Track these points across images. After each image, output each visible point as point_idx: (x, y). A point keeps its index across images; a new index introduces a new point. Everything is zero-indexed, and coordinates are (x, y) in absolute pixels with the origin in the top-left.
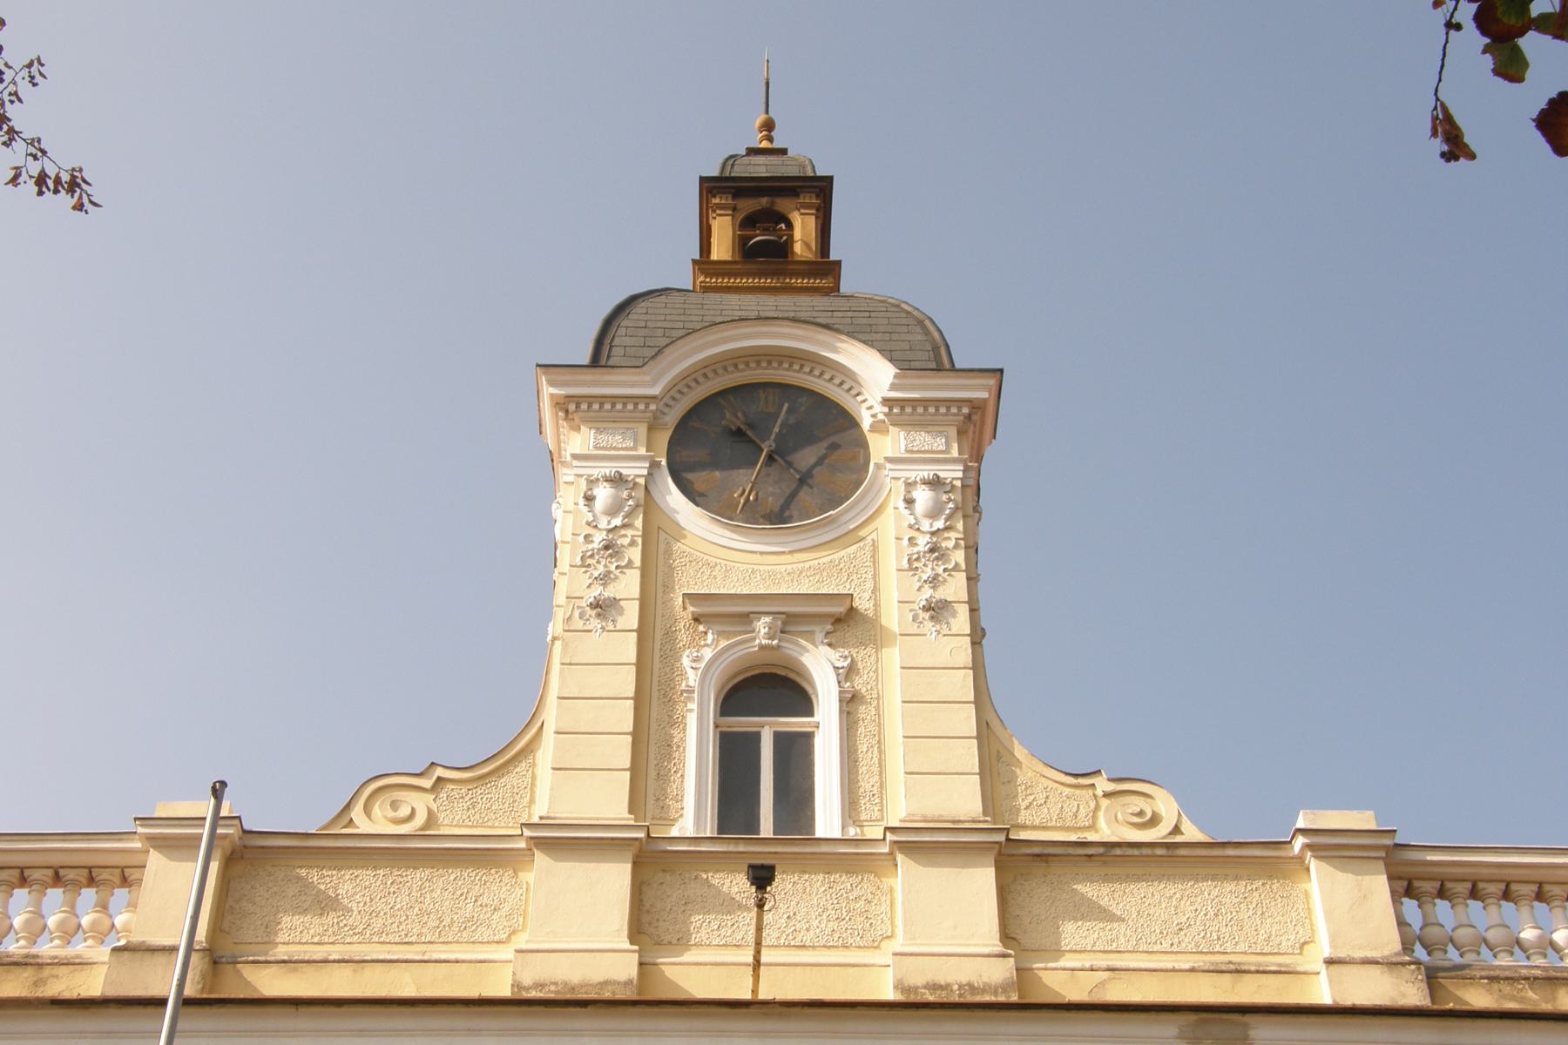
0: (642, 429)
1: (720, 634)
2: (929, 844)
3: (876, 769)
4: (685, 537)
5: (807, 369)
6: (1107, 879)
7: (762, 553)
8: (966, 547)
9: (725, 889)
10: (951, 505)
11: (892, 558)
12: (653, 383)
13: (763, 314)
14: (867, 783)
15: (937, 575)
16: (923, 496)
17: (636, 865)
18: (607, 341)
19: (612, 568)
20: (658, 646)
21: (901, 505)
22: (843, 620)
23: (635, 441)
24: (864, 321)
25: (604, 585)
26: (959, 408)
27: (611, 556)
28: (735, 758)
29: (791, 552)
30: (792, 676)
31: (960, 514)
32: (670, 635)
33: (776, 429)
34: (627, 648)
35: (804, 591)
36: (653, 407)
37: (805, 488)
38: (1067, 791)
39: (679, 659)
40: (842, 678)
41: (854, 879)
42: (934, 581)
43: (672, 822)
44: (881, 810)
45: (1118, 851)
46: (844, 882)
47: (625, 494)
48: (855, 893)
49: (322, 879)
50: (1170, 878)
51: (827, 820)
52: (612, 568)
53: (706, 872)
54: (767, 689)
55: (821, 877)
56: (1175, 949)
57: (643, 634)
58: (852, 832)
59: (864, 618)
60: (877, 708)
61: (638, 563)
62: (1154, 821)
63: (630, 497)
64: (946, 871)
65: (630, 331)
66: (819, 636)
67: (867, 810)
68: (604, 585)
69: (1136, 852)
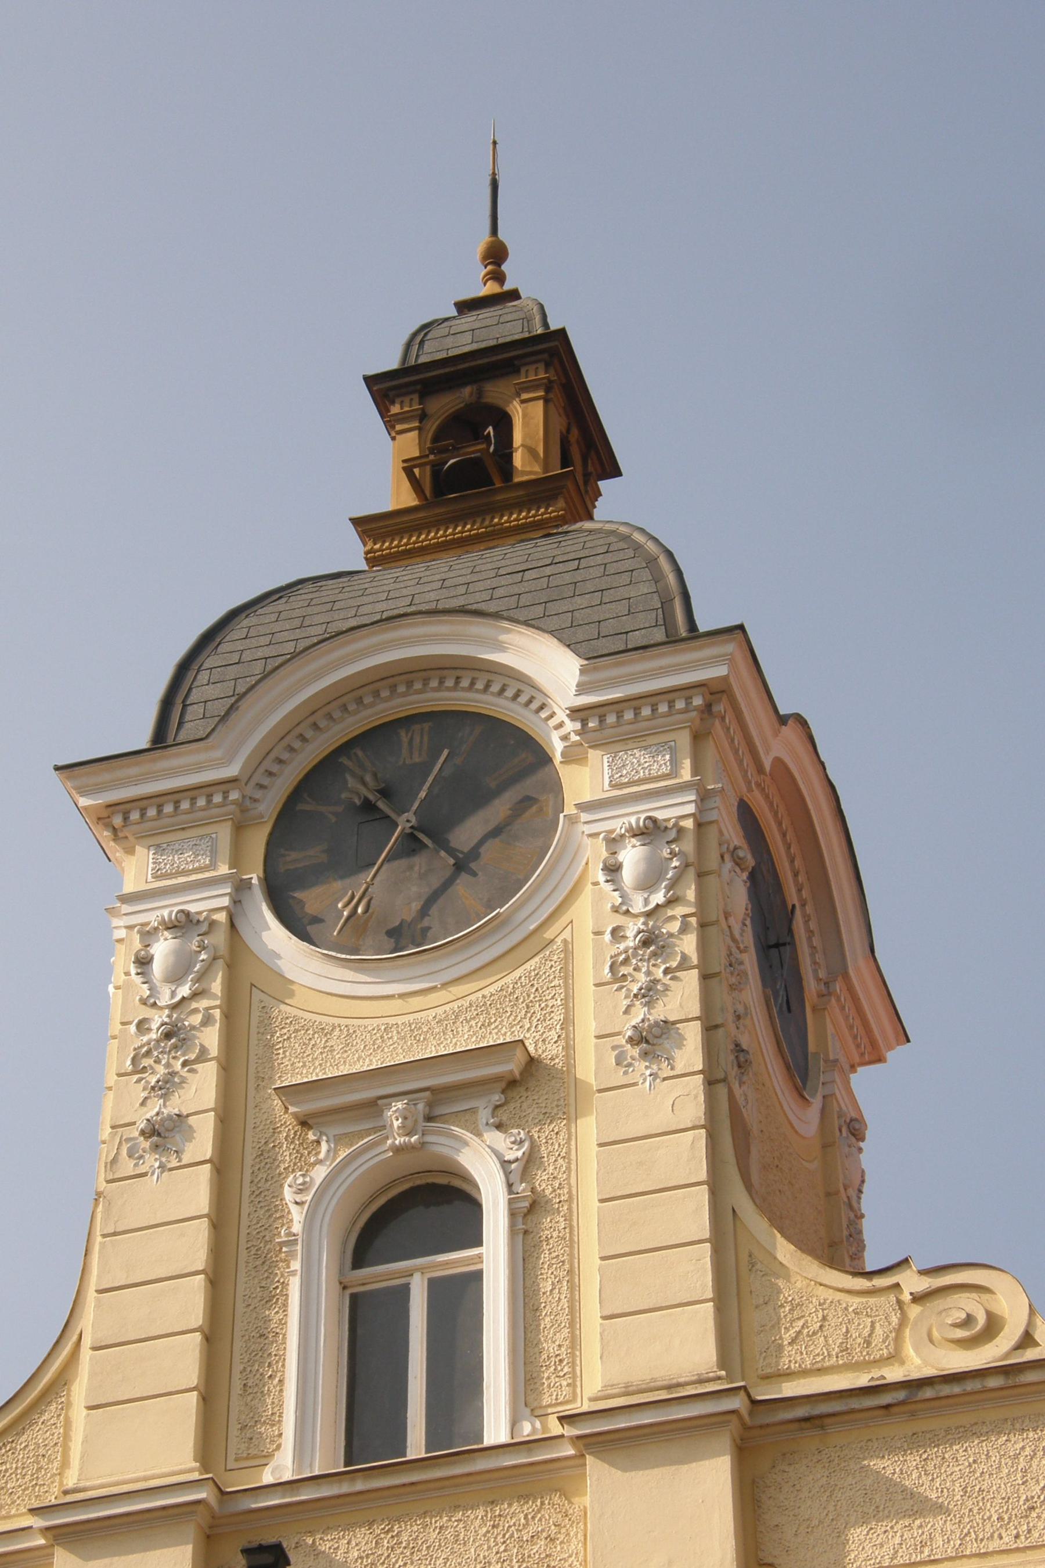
0: (224, 833)
1: (339, 1140)
2: (636, 1431)
3: (564, 1318)
4: (292, 994)
5: (465, 683)
6: (915, 1442)
7: (402, 996)
8: (703, 925)
9: (339, 1556)
10: (675, 863)
11: (589, 967)
12: (229, 760)
13: (334, 628)
14: (552, 1342)
15: (656, 981)
16: (632, 857)
17: (744, 1455)
18: (179, 700)
19: (659, 973)
20: (247, 1177)
21: (601, 877)
22: (518, 1084)
23: (214, 854)
24: (567, 578)
25: (165, 1097)
26: (688, 700)
27: (654, 954)
28: (369, 1332)
29: (445, 985)
30: (457, 1183)
31: (691, 874)
32: (266, 1156)
33: (423, 794)
34: (195, 1192)
35: (358, 1068)
36: (234, 795)
37: (464, 877)
38: (855, 1302)
39: (282, 1186)
40: (515, 1178)
41: (530, 1507)
42: (649, 994)
43: (264, 1458)
44: (572, 1385)
45: (928, 1393)
46: (515, 1512)
47: (665, 853)
48: (531, 1529)
49: (900, 1467)
50: (1014, 1425)
51: (496, 1430)
52: (659, 973)
53: (311, 1533)
54: (421, 1208)
55: (480, 1512)
56: (1022, 1543)
57: (223, 1165)
58: (527, 1429)
59: (551, 1073)
60: (568, 1218)
61: (214, 1050)
62: (993, 1327)
63: (203, 947)
64: (657, 1472)
65: (216, 675)
66: (484, 1115)
67: (554, 1393)
68: (165, 1097)
69: (956, 1389)
